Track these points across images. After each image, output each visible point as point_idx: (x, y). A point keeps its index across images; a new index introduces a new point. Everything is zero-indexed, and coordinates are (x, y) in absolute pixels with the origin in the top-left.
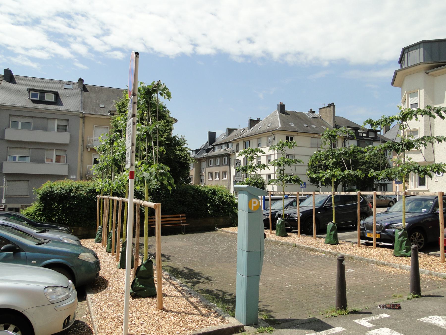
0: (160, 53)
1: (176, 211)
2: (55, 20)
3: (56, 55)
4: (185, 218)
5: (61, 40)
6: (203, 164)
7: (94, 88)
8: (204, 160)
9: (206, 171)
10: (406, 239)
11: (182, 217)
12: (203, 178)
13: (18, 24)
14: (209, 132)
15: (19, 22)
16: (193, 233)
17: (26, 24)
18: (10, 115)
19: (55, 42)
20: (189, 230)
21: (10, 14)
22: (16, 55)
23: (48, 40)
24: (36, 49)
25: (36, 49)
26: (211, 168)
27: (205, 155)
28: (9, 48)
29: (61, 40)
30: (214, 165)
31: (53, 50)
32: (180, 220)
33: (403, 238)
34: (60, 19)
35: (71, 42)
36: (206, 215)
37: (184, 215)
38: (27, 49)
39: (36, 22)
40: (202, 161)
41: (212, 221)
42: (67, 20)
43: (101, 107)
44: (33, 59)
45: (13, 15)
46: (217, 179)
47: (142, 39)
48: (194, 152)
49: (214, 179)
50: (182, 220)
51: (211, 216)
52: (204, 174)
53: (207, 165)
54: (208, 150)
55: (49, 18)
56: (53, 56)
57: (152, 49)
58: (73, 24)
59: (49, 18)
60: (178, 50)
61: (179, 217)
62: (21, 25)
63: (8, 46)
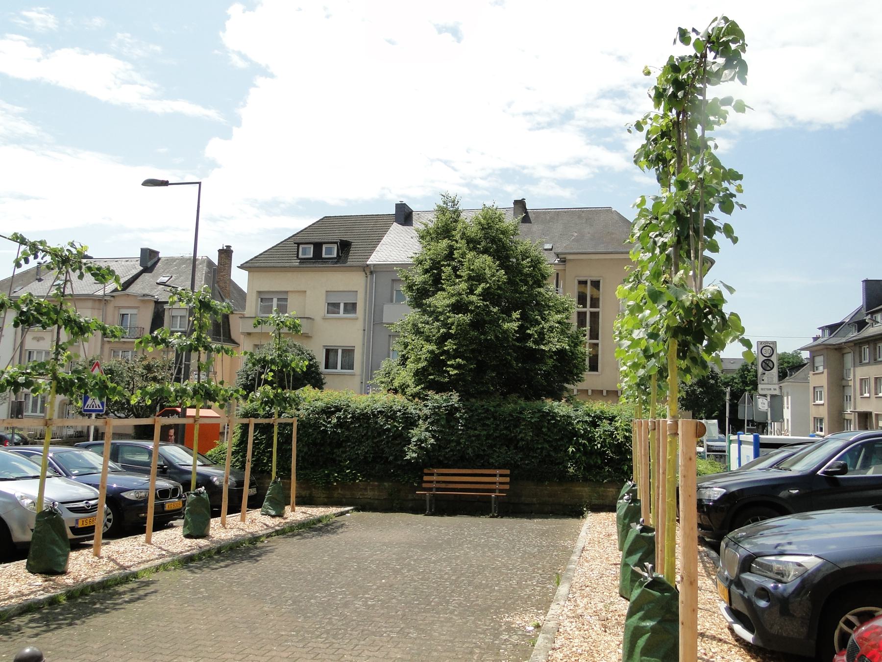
0: (810, 123)
1: (491, 460)
2: (598, 107)
3: (601, 168)
4: (507, 479)
5: (608, 139)
6: (849, 358)
7: (545, 213)
8: (848, 350)
9: (858, 373)
10: (649, 624)
11: (501, 476)
12: (850, 392)
13: (539, 127)
14: (867, 282)
15: (539, 124)
16: (521, 517)
17: (550, 125)
18: (393, 280)
19: (598, 145)
20: (511, 507)
21: (526, 114)
22: (534, 181)
23: (588, 144)
24: (567, 164)
25: (567, 164)
26: (865, 368)
27: (853, 335)
28: (526, 171)
29: (608, 139)
30: (872, 361)
31: (596, 160)
32: (495, 483)
33: (643, 619)
34: (605, 102)
35: (626, 140)
36: (563, 478)
37: (508, 472)
38: (553, 168)
39: (567, 116)
40: (845, 351)
41: (584, 491)
42: (619, 102)
43: (546, 250)
44: (565, 183)
45: (530, 114)
46: (867, 395)
47: (768, 103)
48: (827, 332)
49: (873, 396)
50: (501, 483)
51: (573, 479)
52: (851, 383)
53: (858, 361)
54: (862, 325)
55: (587, 105)
56: (597, 171)
57: (792, 118)
58: (629, 106)
59: (587, 105)
60: (855, 108)
61: (495, 475)
62: (543, 128)
63: (524, 168)
